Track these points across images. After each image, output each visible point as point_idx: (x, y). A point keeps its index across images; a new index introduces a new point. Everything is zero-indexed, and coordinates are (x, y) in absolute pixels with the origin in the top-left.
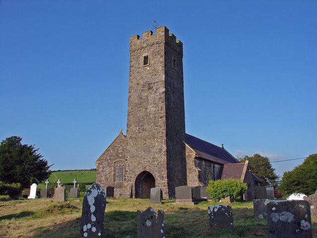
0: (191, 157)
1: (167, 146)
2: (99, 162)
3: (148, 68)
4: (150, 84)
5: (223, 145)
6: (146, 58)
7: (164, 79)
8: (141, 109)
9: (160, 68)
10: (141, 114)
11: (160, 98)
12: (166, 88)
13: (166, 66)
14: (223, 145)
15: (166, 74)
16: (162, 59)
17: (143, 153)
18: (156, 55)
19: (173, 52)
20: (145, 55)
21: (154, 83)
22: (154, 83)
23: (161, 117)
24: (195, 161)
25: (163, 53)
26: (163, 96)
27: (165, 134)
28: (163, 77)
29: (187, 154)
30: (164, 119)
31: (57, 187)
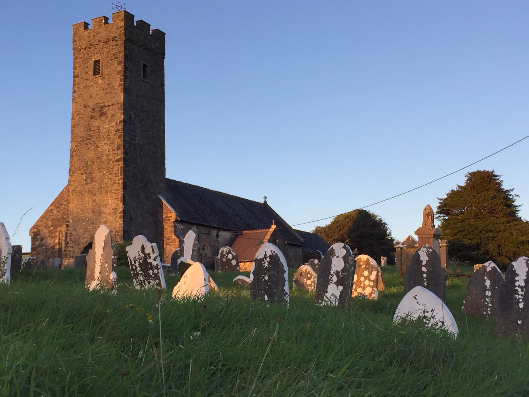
0: (169, 220)
1: (124, 204)
2: (35, 230)
3: (100, 81)
4: (102, 107)
5: (265, 198)
6: (97, 63)
7: (122, 101)
8: (89, 146)
9: (117, 81)
10: (91, 154)
11: (116, 131)
12: (125, 114)
13: (125, 78)
14: (265, 198)
15: (126, 90)
16: (120, 68)
17: (92, 214)
18: (111, 60)
19: (142, 52)
20: (96, 58)
21: (109, 106)
22: (109, 106)
23: (117, 161)
24: (175, 227)
25: (121, 57)
26: (120, 127)
27: (121, 186)
28: (121, 97)
29: (164, 216)
30: (121, 163)
31: (217, 393)
